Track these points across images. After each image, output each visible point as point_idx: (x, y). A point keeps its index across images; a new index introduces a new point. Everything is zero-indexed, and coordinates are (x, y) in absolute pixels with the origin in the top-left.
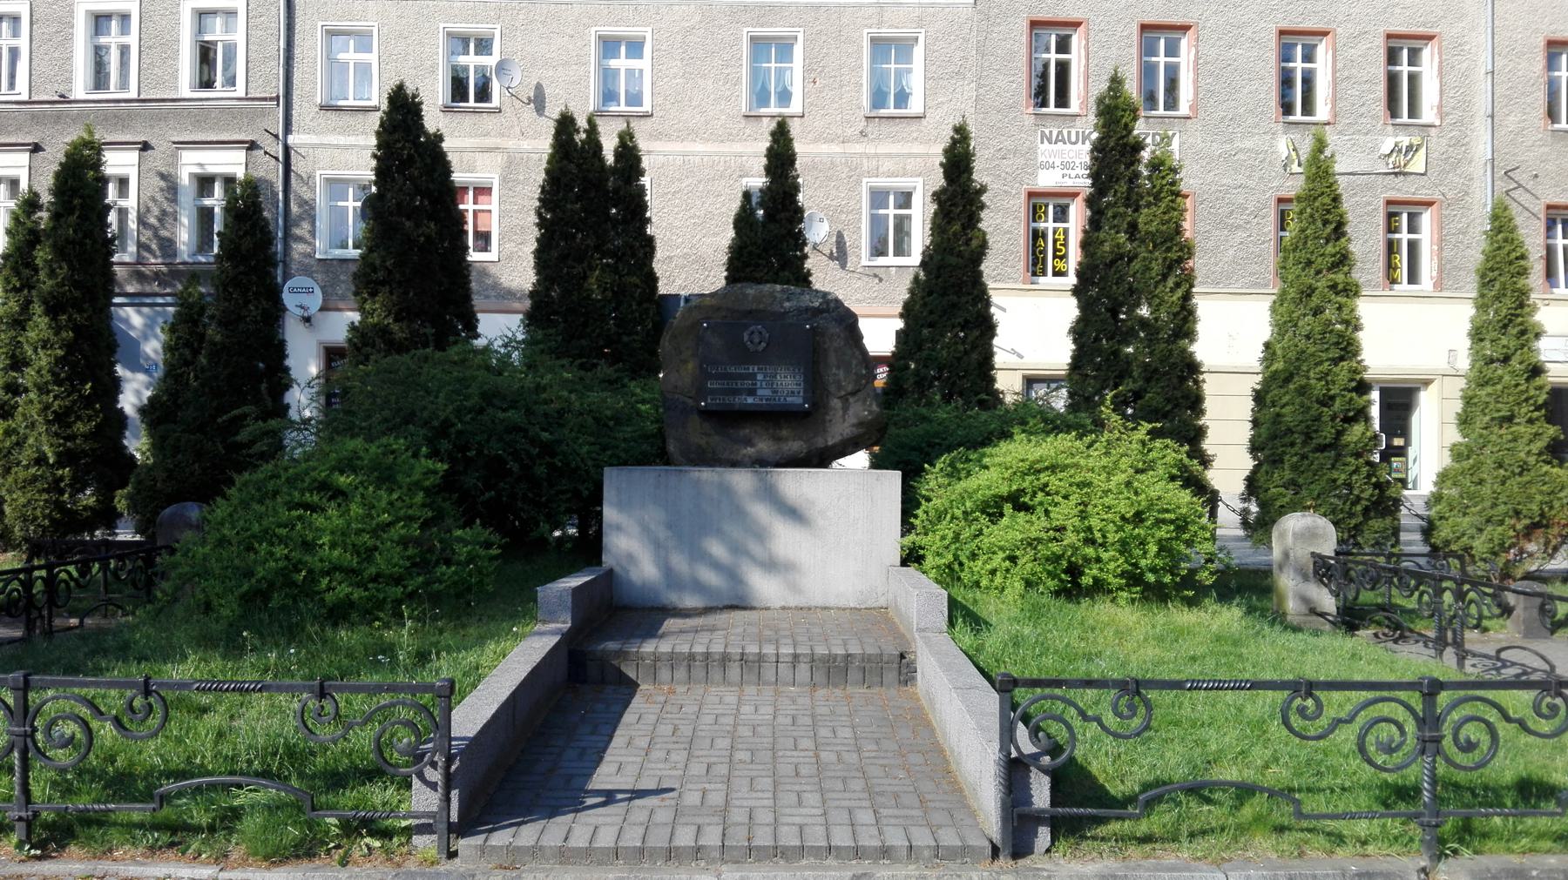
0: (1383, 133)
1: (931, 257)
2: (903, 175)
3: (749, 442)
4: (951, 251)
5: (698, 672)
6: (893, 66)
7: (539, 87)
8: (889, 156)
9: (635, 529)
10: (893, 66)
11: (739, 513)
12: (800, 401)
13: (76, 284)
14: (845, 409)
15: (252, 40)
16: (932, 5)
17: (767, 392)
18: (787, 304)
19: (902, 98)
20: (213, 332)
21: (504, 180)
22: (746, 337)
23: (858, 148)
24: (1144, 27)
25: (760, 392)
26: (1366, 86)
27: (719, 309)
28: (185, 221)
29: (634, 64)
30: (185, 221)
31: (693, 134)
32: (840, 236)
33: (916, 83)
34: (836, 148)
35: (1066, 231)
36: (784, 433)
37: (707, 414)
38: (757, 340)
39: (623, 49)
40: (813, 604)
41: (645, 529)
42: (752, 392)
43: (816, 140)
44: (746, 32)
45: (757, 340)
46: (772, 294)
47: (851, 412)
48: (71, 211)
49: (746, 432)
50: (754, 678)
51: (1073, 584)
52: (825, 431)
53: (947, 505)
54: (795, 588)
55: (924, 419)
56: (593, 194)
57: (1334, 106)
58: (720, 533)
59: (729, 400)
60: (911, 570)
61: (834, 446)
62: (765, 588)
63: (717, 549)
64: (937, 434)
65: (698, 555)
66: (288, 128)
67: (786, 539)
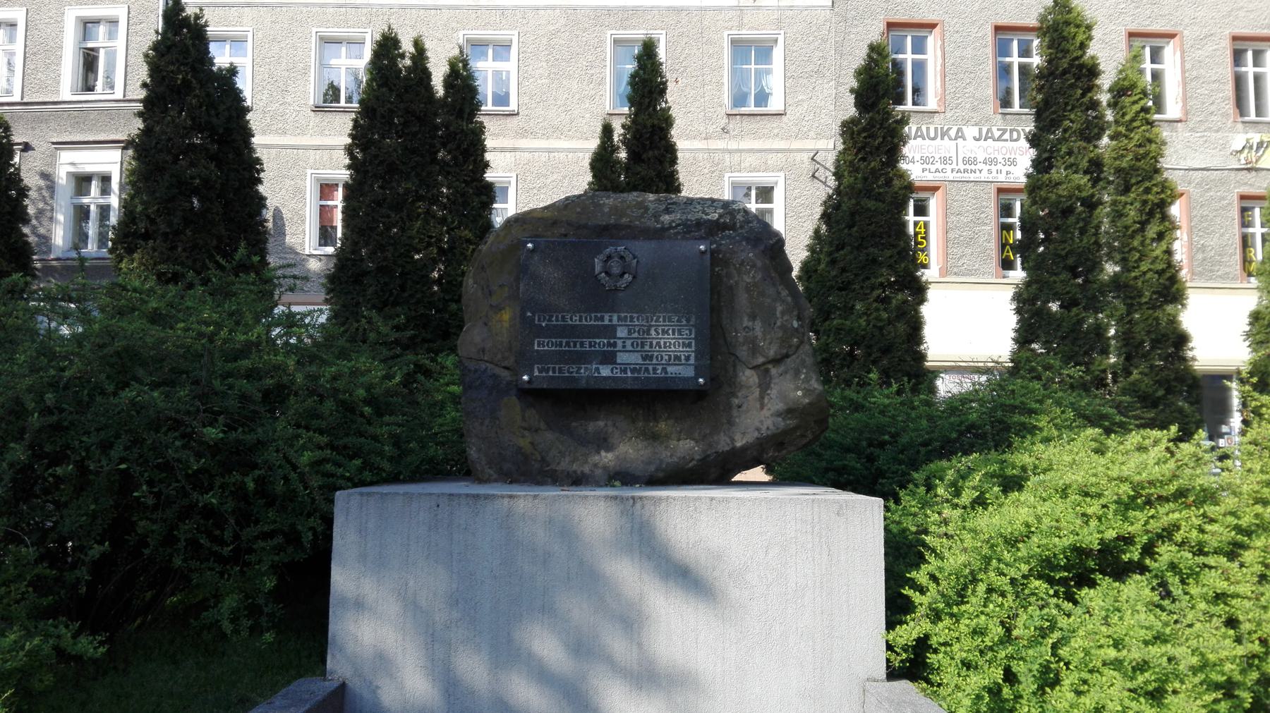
0: (1232, 130)
1: (837, 207)
3: (603, 443)
4: (869, 193)
6: (753, 67)
9: (392, 607)
10: (753, 67)
11: (590, 580)
12: (690, 372)
14: (764, 386)
15: (132, 45)
16: (791, 8)
17: (635, 358)
18: (666, 218)
19: (762, 98)
20: (950, 475)
22: (598, 268)
23: (720, 144)
24: (998, 29)
25: (622, 358)
26: (1215, 86)
27: (555, 223)
28: (61, 217)
29: (500, 65)
30: (61, 217)
31: (557, 131)
33: (775, 83)
35: (926, 225)
36: (663, 426)
37: (532, 395)
38: (616, 270)
39: (490, 52)
41: (411, 606)
42: (609, 358)
44: (609, 35)
45: (616, 270)
46: (642, 206)
47: (773, 392)
52: (731, 423)
53: (977, 565)
55: (857, 407)
56: (416, 124)
57: (1185, 105)
58: (547, 610)
59: (570, 370)
61: (744, 449)
63: (547, 646)
64: (881, 429)
65: (506, 653)
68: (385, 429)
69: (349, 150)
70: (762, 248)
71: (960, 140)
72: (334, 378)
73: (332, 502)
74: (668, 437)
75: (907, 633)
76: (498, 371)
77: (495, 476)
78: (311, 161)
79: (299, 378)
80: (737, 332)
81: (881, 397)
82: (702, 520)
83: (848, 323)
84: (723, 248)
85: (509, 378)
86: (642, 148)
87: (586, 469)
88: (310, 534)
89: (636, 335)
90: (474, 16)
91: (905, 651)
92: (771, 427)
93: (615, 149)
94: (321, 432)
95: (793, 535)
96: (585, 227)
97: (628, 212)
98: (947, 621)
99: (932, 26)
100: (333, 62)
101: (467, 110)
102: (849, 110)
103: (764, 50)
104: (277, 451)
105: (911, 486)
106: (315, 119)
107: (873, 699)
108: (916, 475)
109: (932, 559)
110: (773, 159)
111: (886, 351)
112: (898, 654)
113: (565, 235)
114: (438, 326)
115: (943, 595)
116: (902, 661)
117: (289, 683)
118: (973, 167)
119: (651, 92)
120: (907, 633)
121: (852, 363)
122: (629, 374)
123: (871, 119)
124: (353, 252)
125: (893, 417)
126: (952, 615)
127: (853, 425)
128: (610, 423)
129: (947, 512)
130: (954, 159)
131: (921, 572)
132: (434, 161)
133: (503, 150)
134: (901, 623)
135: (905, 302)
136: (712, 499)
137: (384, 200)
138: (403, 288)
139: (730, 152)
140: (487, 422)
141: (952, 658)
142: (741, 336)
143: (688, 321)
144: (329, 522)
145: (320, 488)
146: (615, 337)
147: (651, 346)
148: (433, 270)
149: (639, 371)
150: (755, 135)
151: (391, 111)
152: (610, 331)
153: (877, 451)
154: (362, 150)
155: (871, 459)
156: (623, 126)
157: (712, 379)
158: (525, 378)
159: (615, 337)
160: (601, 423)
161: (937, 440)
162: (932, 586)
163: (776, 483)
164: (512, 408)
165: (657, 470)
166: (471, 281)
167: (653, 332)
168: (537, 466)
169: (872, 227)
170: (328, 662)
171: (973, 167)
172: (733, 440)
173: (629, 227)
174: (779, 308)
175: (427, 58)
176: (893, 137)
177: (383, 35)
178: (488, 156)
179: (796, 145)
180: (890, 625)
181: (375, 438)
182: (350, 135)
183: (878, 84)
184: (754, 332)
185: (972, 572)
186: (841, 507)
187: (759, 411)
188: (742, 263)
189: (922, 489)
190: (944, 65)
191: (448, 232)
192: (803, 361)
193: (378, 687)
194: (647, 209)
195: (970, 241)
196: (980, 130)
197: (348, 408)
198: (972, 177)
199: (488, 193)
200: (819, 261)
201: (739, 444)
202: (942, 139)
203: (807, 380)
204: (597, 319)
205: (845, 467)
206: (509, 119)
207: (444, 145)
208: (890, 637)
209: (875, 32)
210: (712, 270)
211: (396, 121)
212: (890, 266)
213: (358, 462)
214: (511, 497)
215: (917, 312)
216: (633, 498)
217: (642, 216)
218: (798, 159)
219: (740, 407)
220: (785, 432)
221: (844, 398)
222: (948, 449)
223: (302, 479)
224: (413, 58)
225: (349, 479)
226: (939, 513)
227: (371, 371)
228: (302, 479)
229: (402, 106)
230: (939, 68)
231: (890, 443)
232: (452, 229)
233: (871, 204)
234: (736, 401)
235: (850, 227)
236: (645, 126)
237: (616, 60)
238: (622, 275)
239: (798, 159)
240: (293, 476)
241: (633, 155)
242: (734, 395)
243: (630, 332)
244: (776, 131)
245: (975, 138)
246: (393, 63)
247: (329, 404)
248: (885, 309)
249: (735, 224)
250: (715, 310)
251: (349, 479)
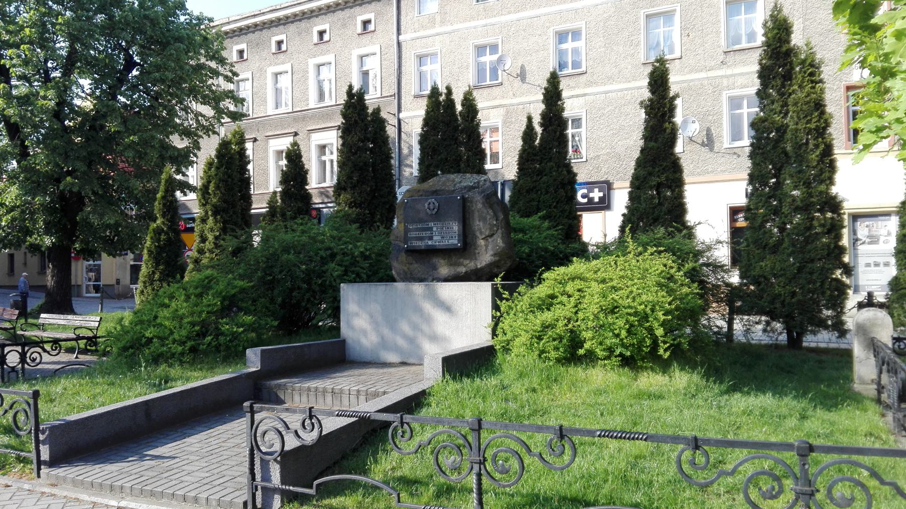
7: (522, 67)
9: (365, 316)
11: (419, 310)
12: (456, 242)
13: (225, 201)
21: (505, 122)
25: (435, 238)
29: (576, 44)
31: (610, 79)
32: (708, 130)
34: (703, 75)
42: (431, 238)
43: (691, 72)
48: (222, 166)
51: (573, 353)
52: (476, 259)
66: (399, 110)
82: (449, 291)
133: (572, 97)
139: (727, 77)
152: (431, 229)
184: (480, 226)
206: (581, 77)
224: (446, 94)
246: (437, 99)
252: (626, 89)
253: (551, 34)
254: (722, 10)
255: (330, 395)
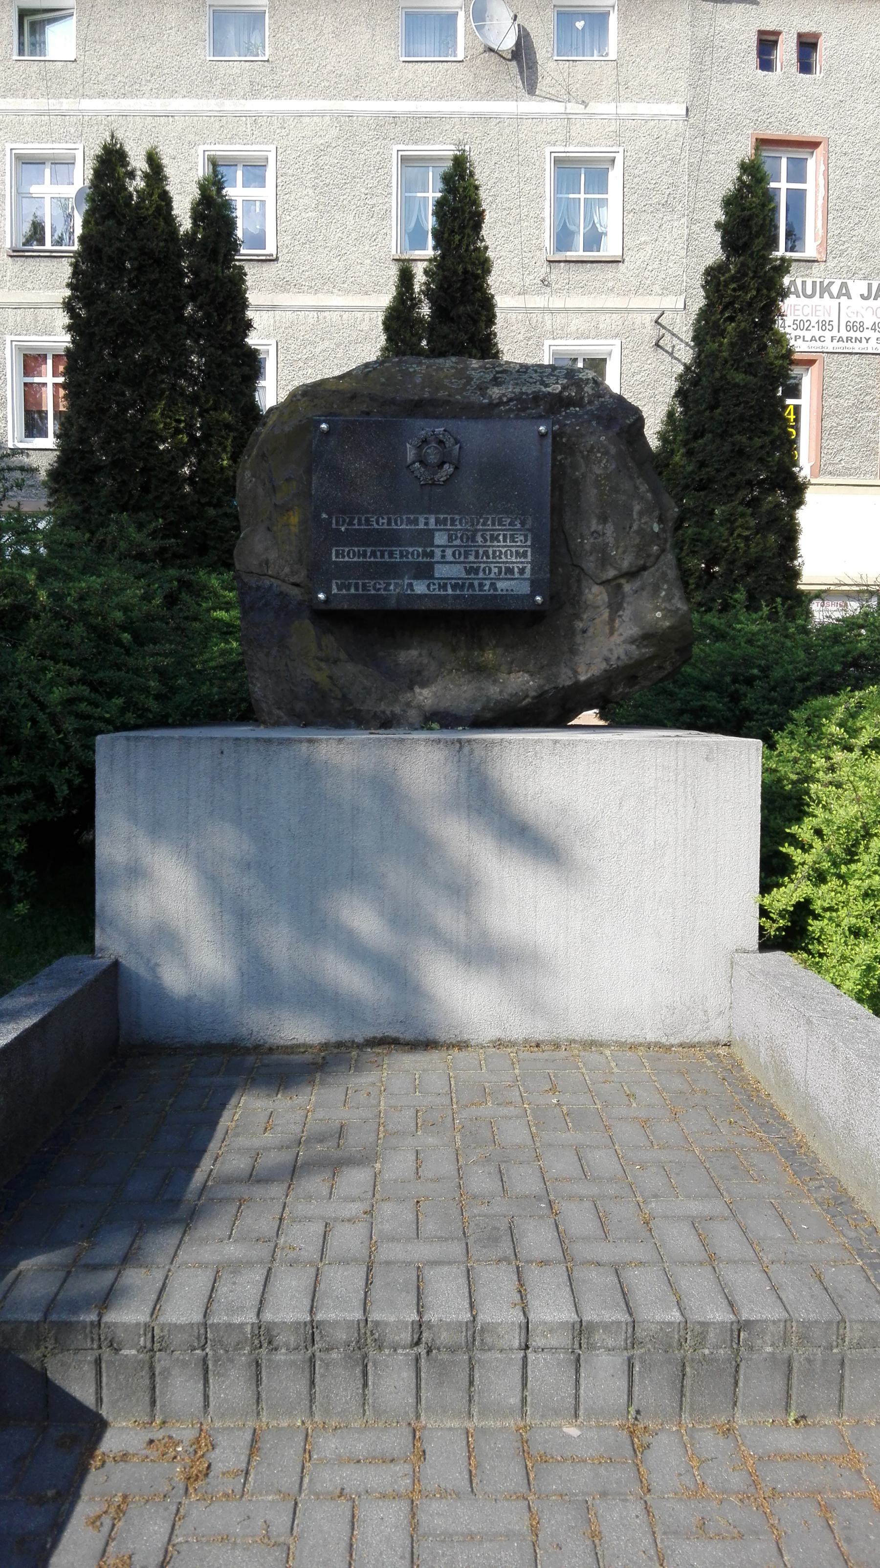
1: (696, 382)
2: (596, 336)
3: (416, 678)
5: (285, 1380)
6: (582, 196)
8: (579, 310)
10: (582, 196)
11: (420, 849)
12: (524, 588)
14: (615, 607)
17: (456, 571)
18: (495, 392)
19: (594, 240)
23: (538, 301)
25: (441, 571)
27: (354, 396)
29: (253, 192)
31: (327, 283)
33: (611, 219)
37: (328, 617)
38: (433, 458)
39: (239, 174)
40: (562, 1033)
42: (425, 571)
44: (395, 150)
45: (433, 458)
47: (627, 613)
49: (410, 655)
50: (455, 1396)
52: (573, 652)
54: (535, 1007)
55: (720, 636)
58: (357, 877)
59: (376, 587)
60: (780, 960)
61: (589, 683)
62: (468, 1001)
63: (363, 919)
64: (747, 662)
65: (317, 927)
67: (517, 898)
68: (149, 660)
69: (68, 306)
70: (616, 429)
71: (844, 299)
72: (82, 598)
73: (92, 748)
74: (497, 669)
75: (785, 897)
76: (287, 588)
77: (285, 718)
78: (11, 324)
79: (43, 596)
80: (582, 538)
81: (749, 624)
83: (706, 532)
84: (568, 430)
85: (300, 598)
86: (449, 302)
87: (397, 710)
88: (65, 787)
89: (457, 542)
90: (217, 125)
91: (783, 917)
92: (623, 656)
93: (416, 304)
94: (71, 664)
95: (652, 784)
96: (393, 402)
97: (446, 382)
98: (834, 883)
99: (813, 145)
100: (35, 189)
101: (223, 251)
102: (712, 250)
103: (596, 173)
104: (20, 687)
105: (790, 727)
106: (13, 267)
107: (744, 973)
108: (795, 715)
109: (819, 811)
110: (606, 322)
111: (750, 568)
112: (774, 921)
113: (368, 414)
114: (203, 533)
115: (829, 853)
116: (778, 929)
117: (50, 963)
118: (858, 335)
119: (463, 228)
120: (785, 897)
121: (708, 582)
122: (450, 591)
123: (743, 264)
124: (81, 441)
125: (764, 647)
126: (840, 876)
127: (714, 657)
128: (424, 652)
129: (838, 756)
130: (835, 324)
131: (804, 827)
132: (180, 318)
134: (779, 886)
135: (778, 505)
136: (556, 742)
137: (117, 373)
138: (145, 489)
139: (552, 311)
140: (274, 651)
141: (838, 925)
142: (588, 542)
143: (523, 524)
144: (89, 773)
145: (77, 731)
146: (432, 545)
147: (477, 557)
148: (183, 466)
149: (462, 587)
150: (584, 289)
151: (121, 252)
152: (426, 537)
153: (743, 688)
154: (86, 306)
155: (735, 698)
156: (426, 272)
157: (552, 598)
158: (321, 596)
159: (432, 545)
160: (414, 653)
161: (816, 674)
162: (817, 843)
163: (609, 727)
164: (305, 634)
165: (483, 709)
166: (248, 474)
167: (479, 539)
168: (337, 705)
169: (740, 409)
170: (97, 936)
171: (858, 335)
172: (575, 673)
173: (447, 402)
174: (637, 508)
175: (166, 178)
176: (769, 289)
177: (105, 148)
178: (250, 314)
179: (637, 302)
180: (765, 889)
181: (137, 671)
182: (69, 285)
183: (750, 218)
184: (613, 533)
185: (865, 826)
186: (711, 751)
187: (606, 641)
188: (591, 450)
189: (803, 731)
190: (827, 198)
191: (201, 415)
192: (664, 574)
193: (157, 965)
194: (469, 379)
195: (851, 432)
196: (870, 286)
197: (102, 635)
198: (857, 347)
199: (250, 365)
200: (672, 452)
201: (582, 678)
202: (821, 297)
203: (669, 598)
204: (409, 522)
205: (703, 708)
206: (266, 266)
207: (193, 298)
208: (767, 901)
209: (745, 150)
210: (554, 459)
211: (128, 265)
212: (761, 460)
213: (119, 701)
214: (310, 741)
215: (792, 517)
216: (459, 741)
217: (464, 389)
218: (638, 322)
219: (584, 631)
220: (640, 663)
221: (703, 624)
222: (829, 685)
223: (53, 719)
224: (146, 176)
225: (108, 721)
226: (828, 758)
227: (127, 592)
228: (53, 719)
229: (135, 245)
230: (820, 202)
231: (760, 679)
232: (207, 411)
233: (739, 378)
234: (580, 625)
235: (712, 408)
236: (455, 272)
237: (408, 185)
238: (441, 465)
239: (638, 322)
240: (41, 716)
241: (439, 310)
242: (577, 616)
243: (450, 539)
244: (610, 284)
245: (862, 296)
247: (79, 630)
248: (752, 515)
249: (582, 398)
250: (557, 510)
251: (108, 721)
252: (361, 309)
253: (200, 160)
254: (547, 173)
255: (403, 1357)
